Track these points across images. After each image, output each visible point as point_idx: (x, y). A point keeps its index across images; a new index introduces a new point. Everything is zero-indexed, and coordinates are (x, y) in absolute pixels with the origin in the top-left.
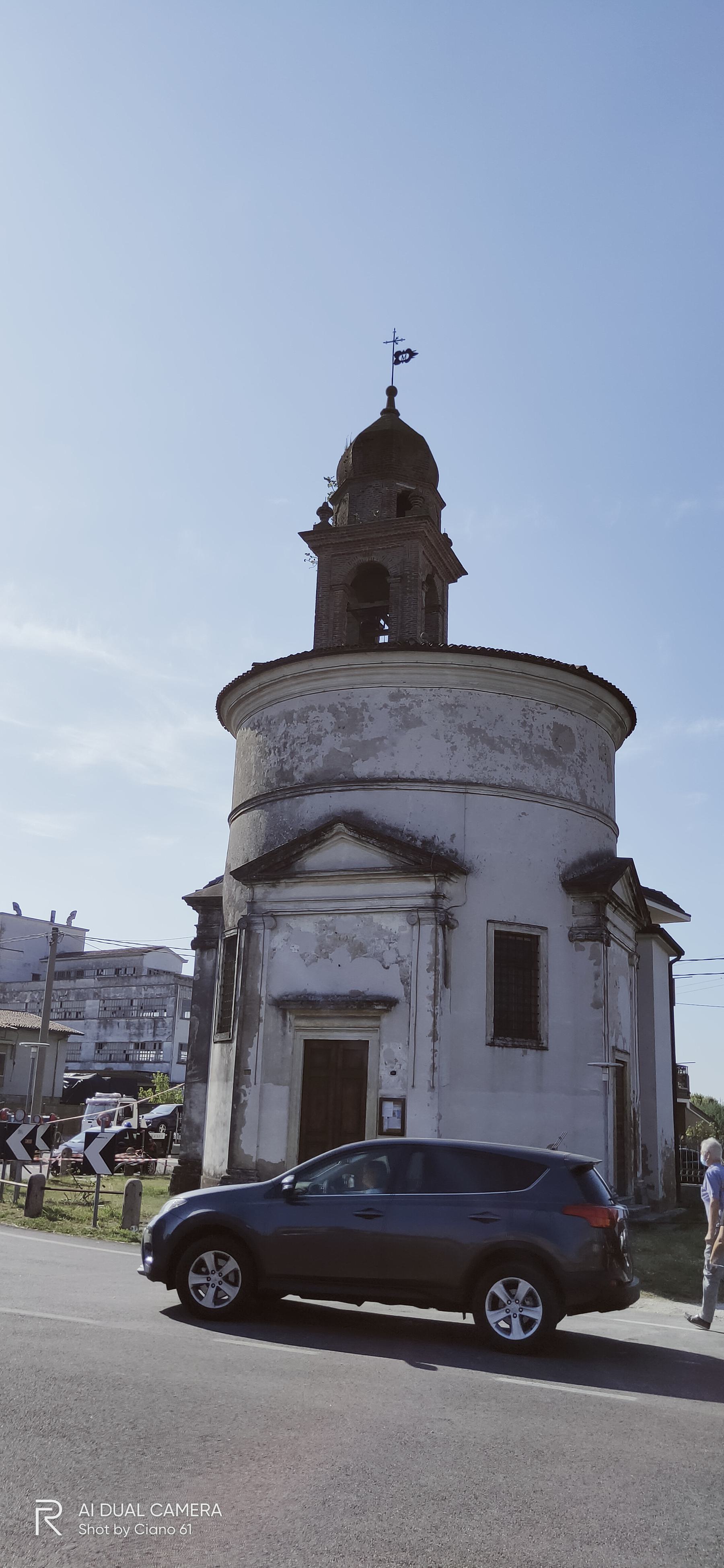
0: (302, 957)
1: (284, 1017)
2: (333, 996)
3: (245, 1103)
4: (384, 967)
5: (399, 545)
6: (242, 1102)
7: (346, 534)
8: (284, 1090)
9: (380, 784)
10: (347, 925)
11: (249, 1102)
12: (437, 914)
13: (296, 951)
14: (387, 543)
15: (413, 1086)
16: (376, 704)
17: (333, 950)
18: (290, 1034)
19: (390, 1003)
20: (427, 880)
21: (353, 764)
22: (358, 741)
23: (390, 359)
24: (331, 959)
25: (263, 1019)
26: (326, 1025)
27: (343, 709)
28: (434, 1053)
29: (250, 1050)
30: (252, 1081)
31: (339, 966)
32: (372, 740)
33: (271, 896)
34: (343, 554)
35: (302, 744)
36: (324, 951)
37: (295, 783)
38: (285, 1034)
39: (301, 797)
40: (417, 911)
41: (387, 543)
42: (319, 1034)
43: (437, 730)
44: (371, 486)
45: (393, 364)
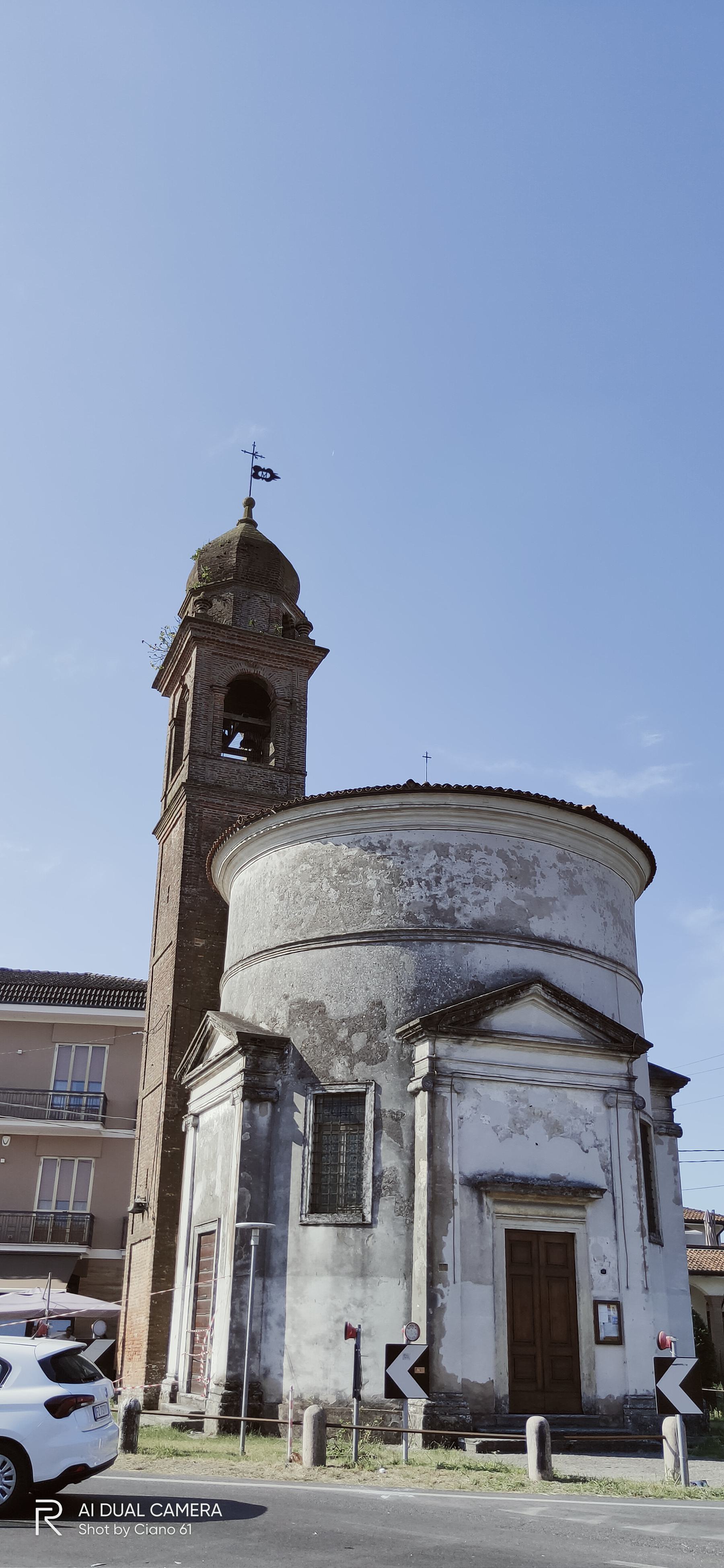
0: (495, 1131)
1: (480, 1201)
2: (532, 1179)
3: (443, 1307)
4: (584, 1151)
5: (288, 668)
6: (439, 1305)
7: (237, 636)
8: (486, 1291)
9: (559, 948)
10: (539, 1097)
11: (448, 1307)
12: (635, 1098)
13: (488, 1123)
14: (275, 661)
15: (627, 1287)
16: (546, 861)
17: (528, 1126)
18: (488, 1222)
19: (602, 1191)
20: (620, 1059)
21: (529, 920)
22: (531, 896)
23: (249, 472)
24: (527, 1136)
25: (458, 1201)
26: (529, 1213)
27: (514, 858)
28: (644, 1249)
29: (444, 1238)
30: (450, 1279)
31: (537, 1144)
32: (545, 898)
33: (455, 1053)
34: (226, 656)
35: (466, 884)
36: (518, 1125)
37: (458, 926)
38: (482, 1221)
39: (469, 944)
40: (617, 1093)
41: (275, 661)
42: (521, 1223)
43: (594, 902)
44: (258, 596)
45: (252, 476)
